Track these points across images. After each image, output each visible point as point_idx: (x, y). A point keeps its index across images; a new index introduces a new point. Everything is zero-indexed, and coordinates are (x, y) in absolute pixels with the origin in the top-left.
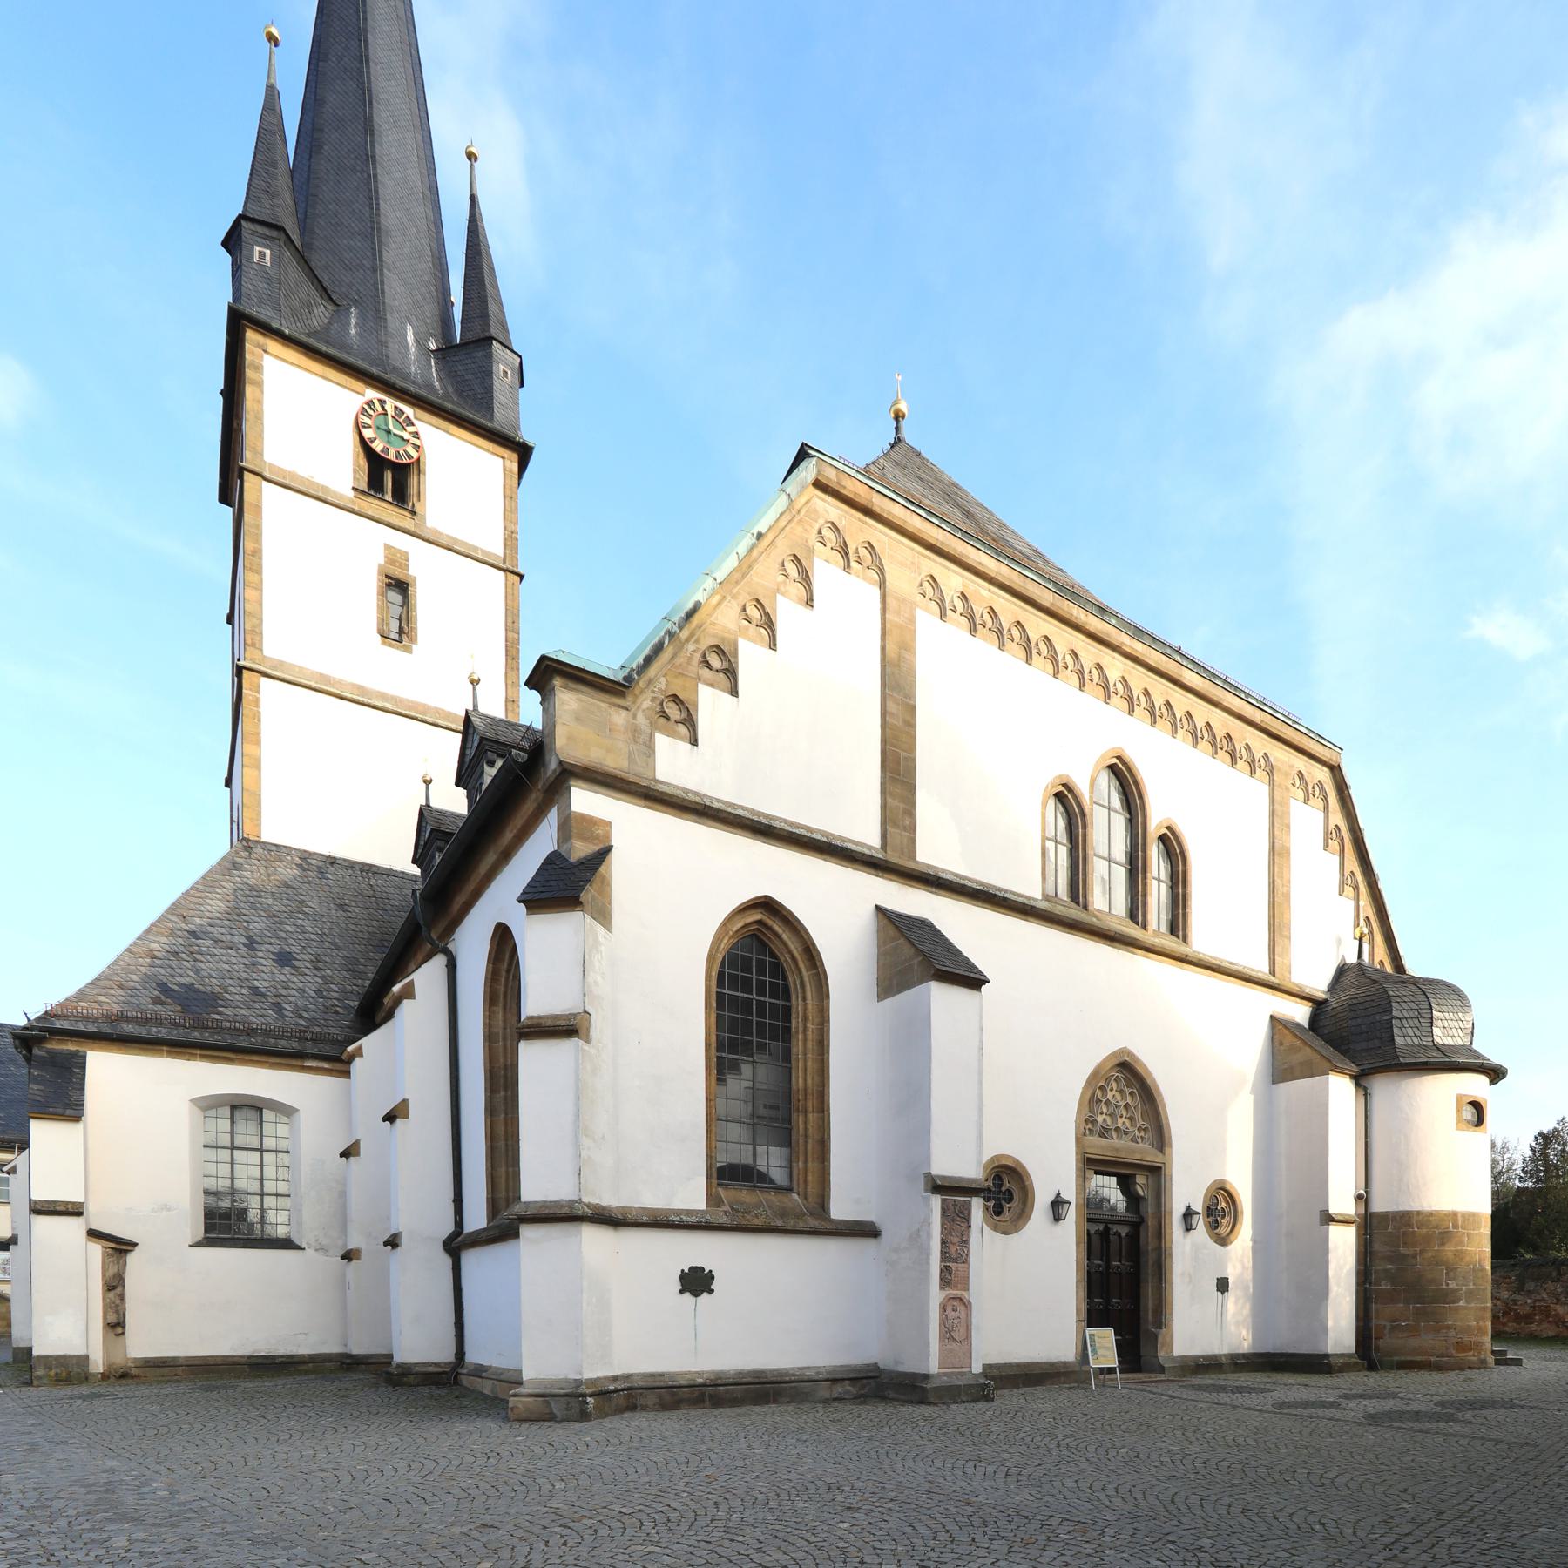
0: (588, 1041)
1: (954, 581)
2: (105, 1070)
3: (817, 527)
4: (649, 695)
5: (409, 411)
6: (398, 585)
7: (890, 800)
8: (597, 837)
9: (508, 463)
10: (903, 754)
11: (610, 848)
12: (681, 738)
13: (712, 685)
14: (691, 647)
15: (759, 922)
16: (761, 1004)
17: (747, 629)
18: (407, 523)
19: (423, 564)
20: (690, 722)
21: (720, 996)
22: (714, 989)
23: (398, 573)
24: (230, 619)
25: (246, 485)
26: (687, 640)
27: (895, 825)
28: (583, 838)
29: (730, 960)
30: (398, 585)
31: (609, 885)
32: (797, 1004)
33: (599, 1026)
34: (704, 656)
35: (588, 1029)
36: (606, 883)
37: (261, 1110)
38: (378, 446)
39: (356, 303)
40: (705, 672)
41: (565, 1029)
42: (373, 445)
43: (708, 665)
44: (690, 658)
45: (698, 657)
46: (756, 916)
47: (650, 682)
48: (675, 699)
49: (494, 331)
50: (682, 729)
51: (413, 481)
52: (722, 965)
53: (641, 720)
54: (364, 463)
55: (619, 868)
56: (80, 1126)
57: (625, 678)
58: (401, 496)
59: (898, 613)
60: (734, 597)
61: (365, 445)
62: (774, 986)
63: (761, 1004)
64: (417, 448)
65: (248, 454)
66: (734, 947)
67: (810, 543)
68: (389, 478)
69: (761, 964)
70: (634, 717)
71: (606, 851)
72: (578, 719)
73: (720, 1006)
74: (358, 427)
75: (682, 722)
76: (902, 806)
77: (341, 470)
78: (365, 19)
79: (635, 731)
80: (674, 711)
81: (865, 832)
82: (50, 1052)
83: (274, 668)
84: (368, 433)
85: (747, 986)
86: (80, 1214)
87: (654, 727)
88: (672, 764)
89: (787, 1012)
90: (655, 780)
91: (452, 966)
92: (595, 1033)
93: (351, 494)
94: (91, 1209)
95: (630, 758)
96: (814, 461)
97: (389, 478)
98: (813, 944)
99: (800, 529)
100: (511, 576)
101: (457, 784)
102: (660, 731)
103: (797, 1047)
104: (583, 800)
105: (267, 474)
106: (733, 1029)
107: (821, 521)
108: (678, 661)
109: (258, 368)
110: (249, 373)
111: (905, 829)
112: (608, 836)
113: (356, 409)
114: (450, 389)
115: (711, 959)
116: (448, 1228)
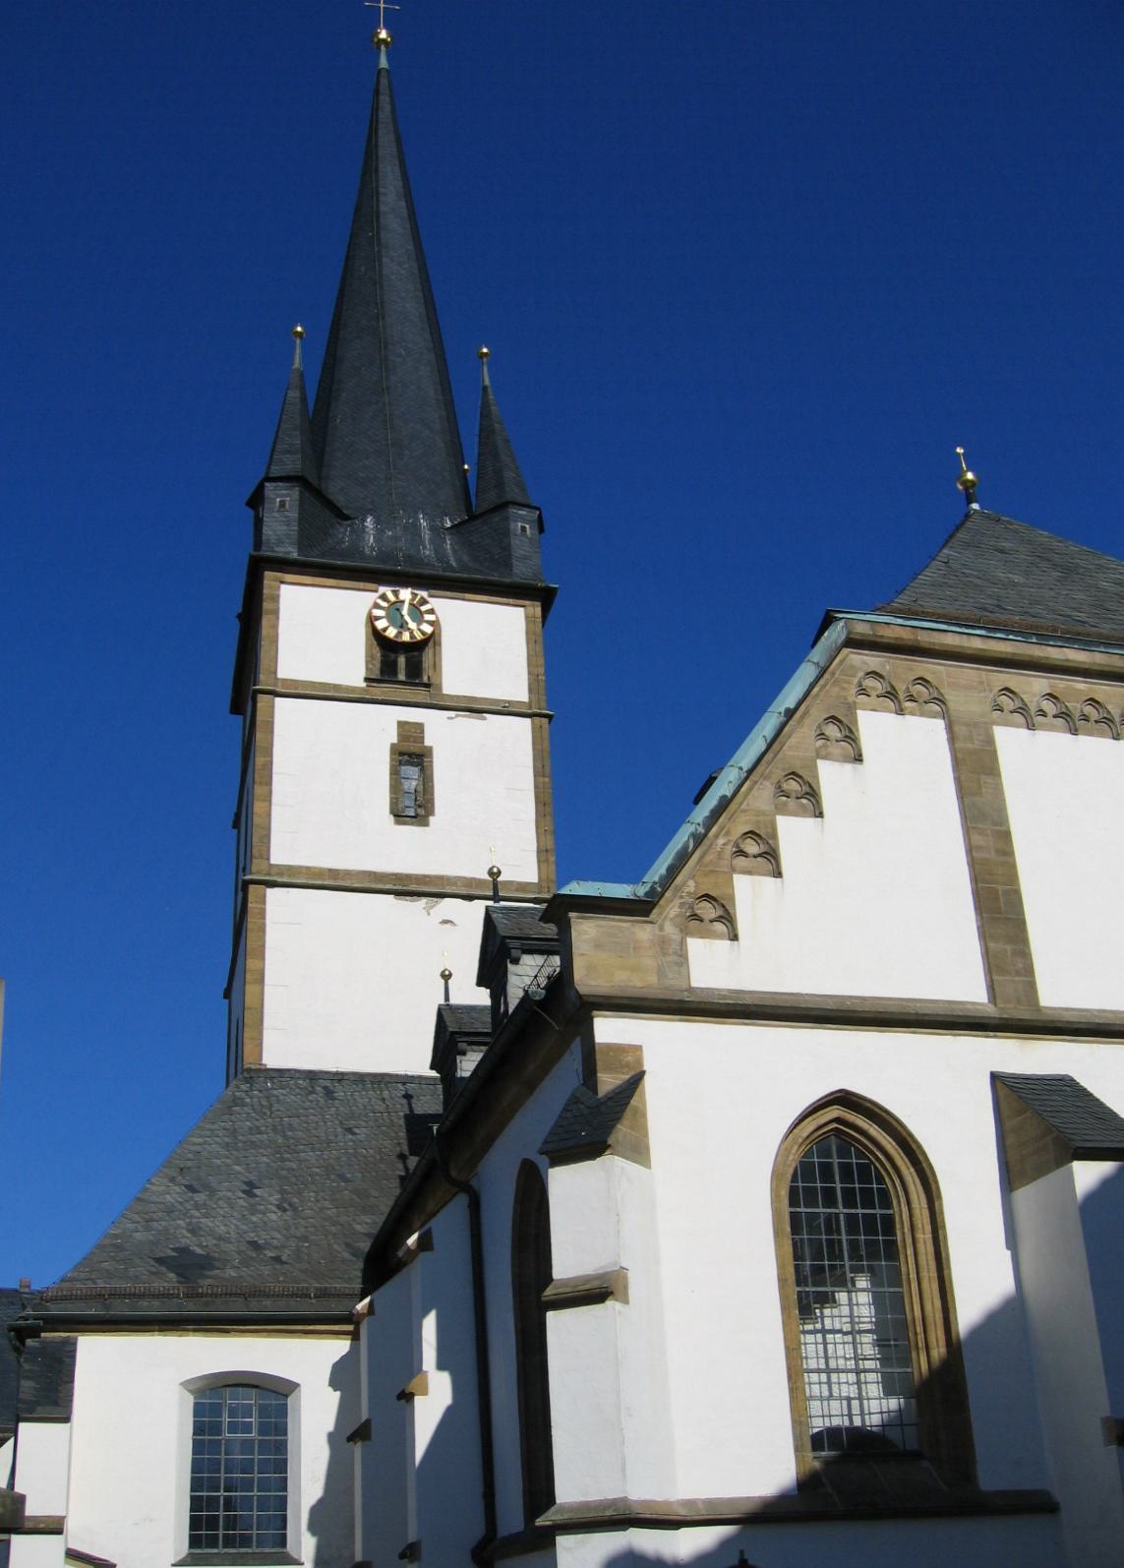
0: (626, 1301)
1: (1033, 686)
2: (97, 1357)
3: (856, 681)
4: (677, 901)
5: (424, 594)
6: (411, 756)
7: (992, 945)
8: (627, 1065)
9: (531, 610)
10: (1000, 888)
11: (642, 1074)
12: (719, 937)
13: (749, 873)
14: (721, 841)
15: (838, 1120)
16: (851, 1220)
17: (785, 804)
18: (420, 695)
19: (438, 728)
20: (728, 918)
21: (795, 1219)
22: (786, 1210)
23: (413, 748)
24: (236, 824)
25: (259, 705)
26: (717, 836)
27: (1002, 971)
28: (609, 1069)
29: (804, 1170)
30: (411, 756)
31: (644, 1115)
32: (900, 1210)
33: (636, 1287)
34: (737, 846)
35: (626, 1287)
36: (641, 1114)
37: (246, 884)
38: (391, 633)
39: (370, 512)
40: (741, 861)
41: (596, 1292)
42: (387, 634)
43: (741, 853)
44: (720, 854)
45: (730, 849)
46: (835, 1112)
47: (679, 889)
48: (708, 897)
49: (512, 492)
50: (720, 927)
51: (427, 656)
52: (794, 1178)
53: (670, 929)
54: (377, 653)
55: (654, 1095)
56: (68, 1425)
57: (646, 894)
58: (415, 673)
59: (970, 739)
60: (766, 778)
61: (378, 636)
62: (867, 1194)
63: (851, 1220)
64: (431, 623)
65: (262, 677)
66: (808, 1154)
67: (850, 699)
68: (401, 665)
69: (846, 1170)
70: (661, 928)
71: (637, 1079)
72: (598, 946)
73: (796, 1227)
74: (371, 620)
75: (719, 919)
76: (1009, 948)
77: (352, 666)
78: (382, 287)
79: (663, 943)
80: (708, 911)
81: (965, 983)
82: (46, 1343)
83: (281, 874)
84: (380, 624)
85: (830, 1199)
86: (59, 1532)
87: (686, 932)
88: (711, 965)
89: (889, 1224)
90: (690, 989)
91: (475, 1206)
92: (632, 1292)
93: (364, 685)
94: (70, 1526)
95: (661, 973)
96: (841, 624)
97: (401, 665)
98: (911, 1135)
99: (836, 689)
100: (537, 719)
101: (480, 983)
102: (692, 935)
103: (908, 1266)
104: (608, 1029)
105: (279, 690)
106: (817, 1255)
107: (861, 674)
108: (708, 858)
109: (276, 599)
110: (266, 605)
111: (1018, 973)
112: (639, 1061)
113: (371, 604)
114: (466, 558)
115: (776, 1175)
116: (478, 1531)
